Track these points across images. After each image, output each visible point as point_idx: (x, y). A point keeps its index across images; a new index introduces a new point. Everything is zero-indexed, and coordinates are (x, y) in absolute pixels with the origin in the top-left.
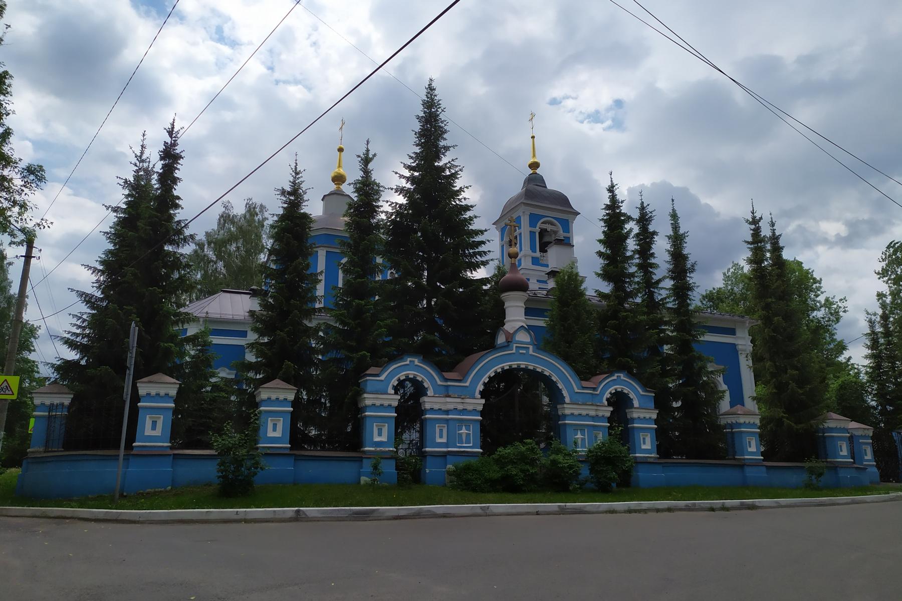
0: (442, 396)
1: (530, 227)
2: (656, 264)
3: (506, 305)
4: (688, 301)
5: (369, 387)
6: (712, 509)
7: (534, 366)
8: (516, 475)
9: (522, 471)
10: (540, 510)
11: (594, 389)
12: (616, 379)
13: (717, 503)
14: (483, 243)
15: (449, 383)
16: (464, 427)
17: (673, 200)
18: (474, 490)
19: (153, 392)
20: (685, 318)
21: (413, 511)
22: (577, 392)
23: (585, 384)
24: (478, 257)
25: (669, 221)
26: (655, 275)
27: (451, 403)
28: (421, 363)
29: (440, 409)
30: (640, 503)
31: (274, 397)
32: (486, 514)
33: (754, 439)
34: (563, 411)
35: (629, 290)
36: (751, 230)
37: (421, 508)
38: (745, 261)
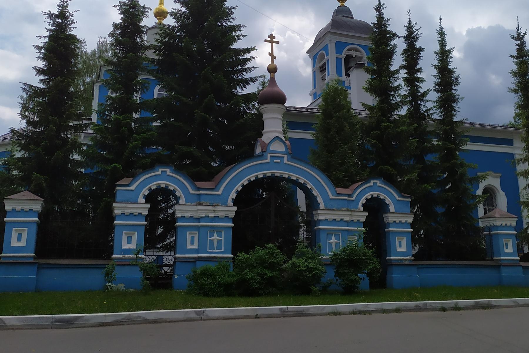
0: (194, 204)
1: (336, 54)
2: (421, 78)
3: (265, 117)
4: (453, 112)
5: (118, 197)
6: (443, 309)
7: (289, 174)
8: (252, 279)
9: (259, 274)
10: (259, 313)
11: (349, 195)
12: (372, 186)
13: (450, 303)
14: (249, 60)
15: (201, 192)
16: (215, 233)
17: (441, 19)
18: (206, 295)
19: (504, 224)
20: (447, 128)
21: (121, 318)
22: (331, 199)
23: (340, 190)
24: (245, 73)
25: (436, 38)
26: (422, 88)
27: (202, 211)
28: (173, 173)
29: (342, 220)
30: (367, 305)
31: (18, 208)
32: (201, 318)
33: (511, 241)
34: (317, 217)
35: (393, 102)
36: (517, 45)
37: (130, 314)
38: (511, 75)
